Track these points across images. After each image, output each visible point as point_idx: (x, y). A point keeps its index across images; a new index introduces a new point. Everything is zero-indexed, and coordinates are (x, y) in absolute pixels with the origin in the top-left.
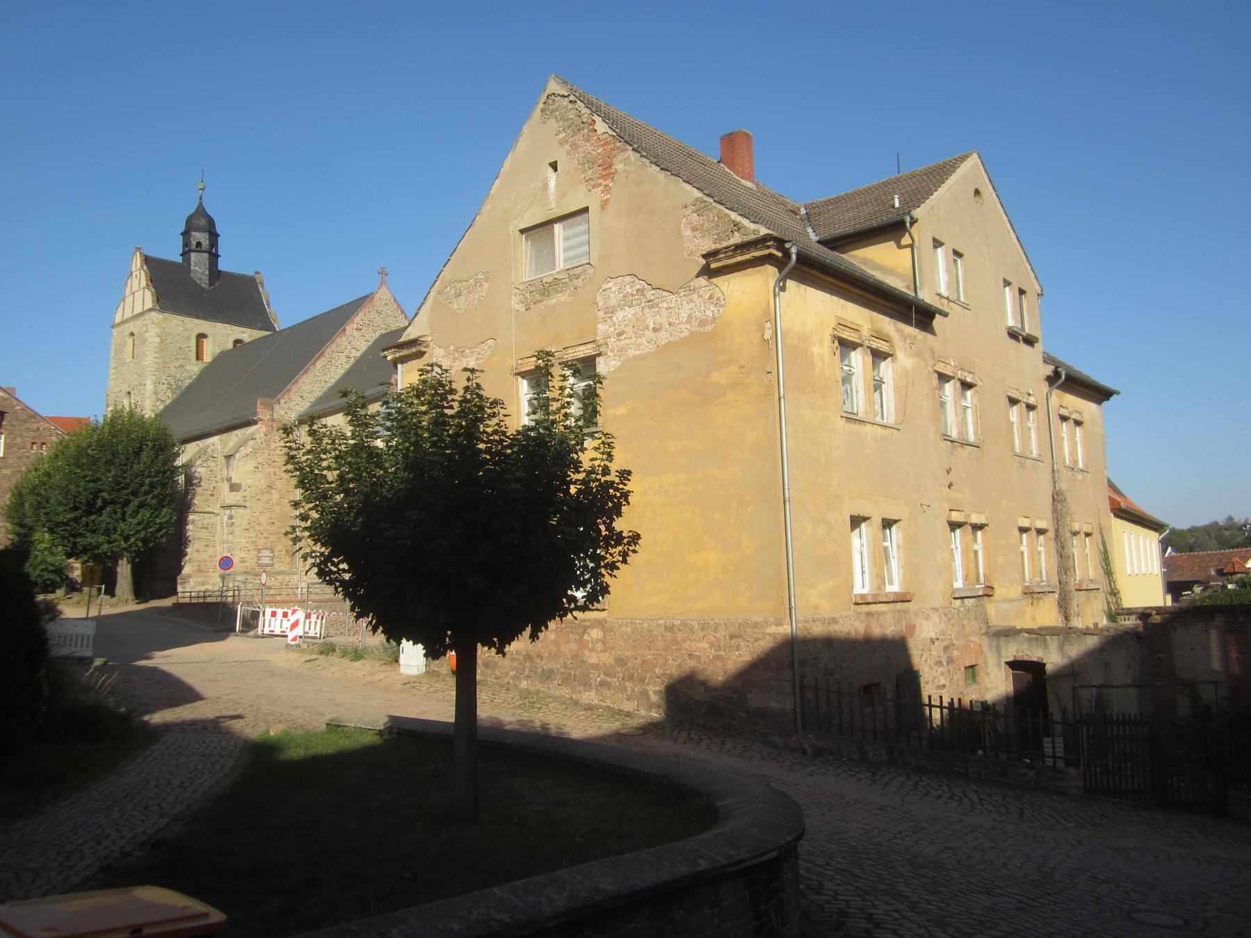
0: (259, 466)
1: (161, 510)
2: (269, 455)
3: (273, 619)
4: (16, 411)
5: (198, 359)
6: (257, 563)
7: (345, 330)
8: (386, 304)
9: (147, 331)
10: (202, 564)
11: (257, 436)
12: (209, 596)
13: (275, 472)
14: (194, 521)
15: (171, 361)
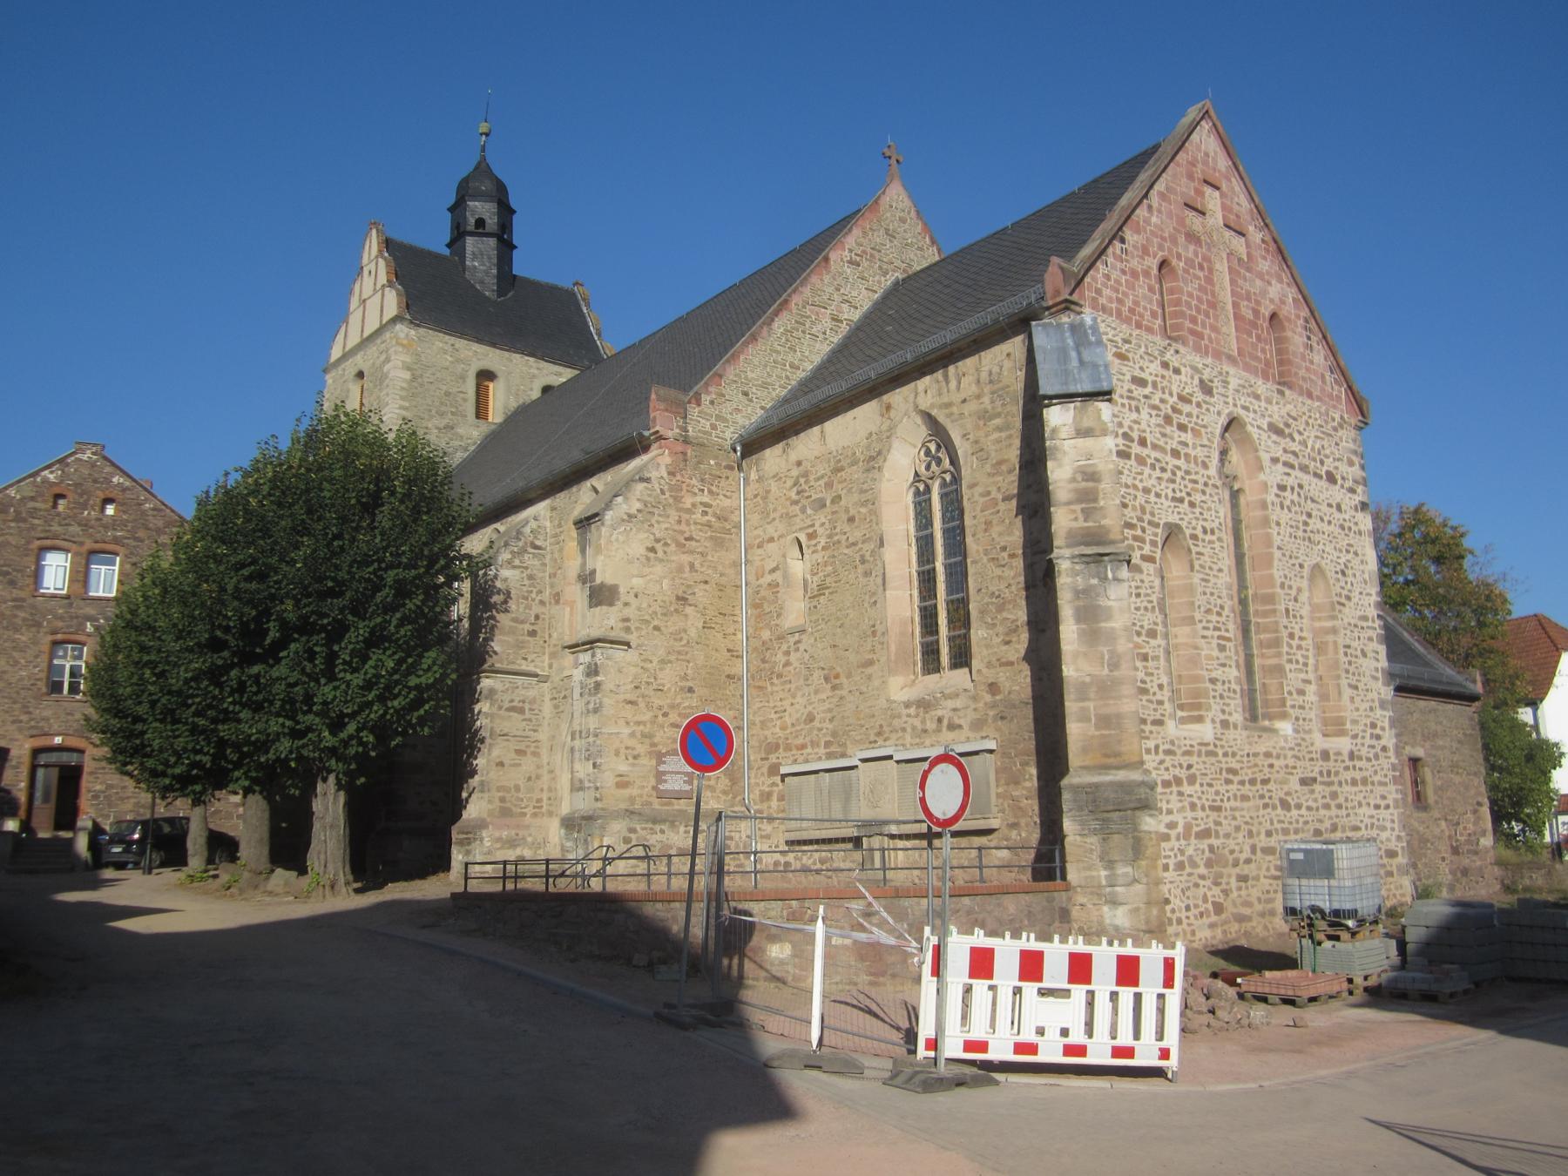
0: (658, 547)
1: (421, 656)
2: (679, 522)
3: (980, 986)
4: (144, 513)
5: (478, 417)
6: (655, 788)
7: (826, 259)
8: (903, 220)
9: (388, 360)
10: (508, 796)
11: (654, 474)
12: (562, 875)
13: (692, 566)
14: (492, 691)
15: (432, 417)
